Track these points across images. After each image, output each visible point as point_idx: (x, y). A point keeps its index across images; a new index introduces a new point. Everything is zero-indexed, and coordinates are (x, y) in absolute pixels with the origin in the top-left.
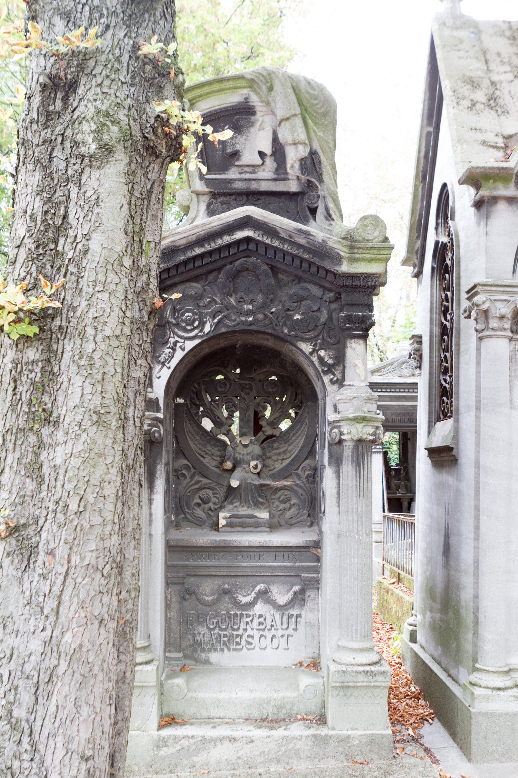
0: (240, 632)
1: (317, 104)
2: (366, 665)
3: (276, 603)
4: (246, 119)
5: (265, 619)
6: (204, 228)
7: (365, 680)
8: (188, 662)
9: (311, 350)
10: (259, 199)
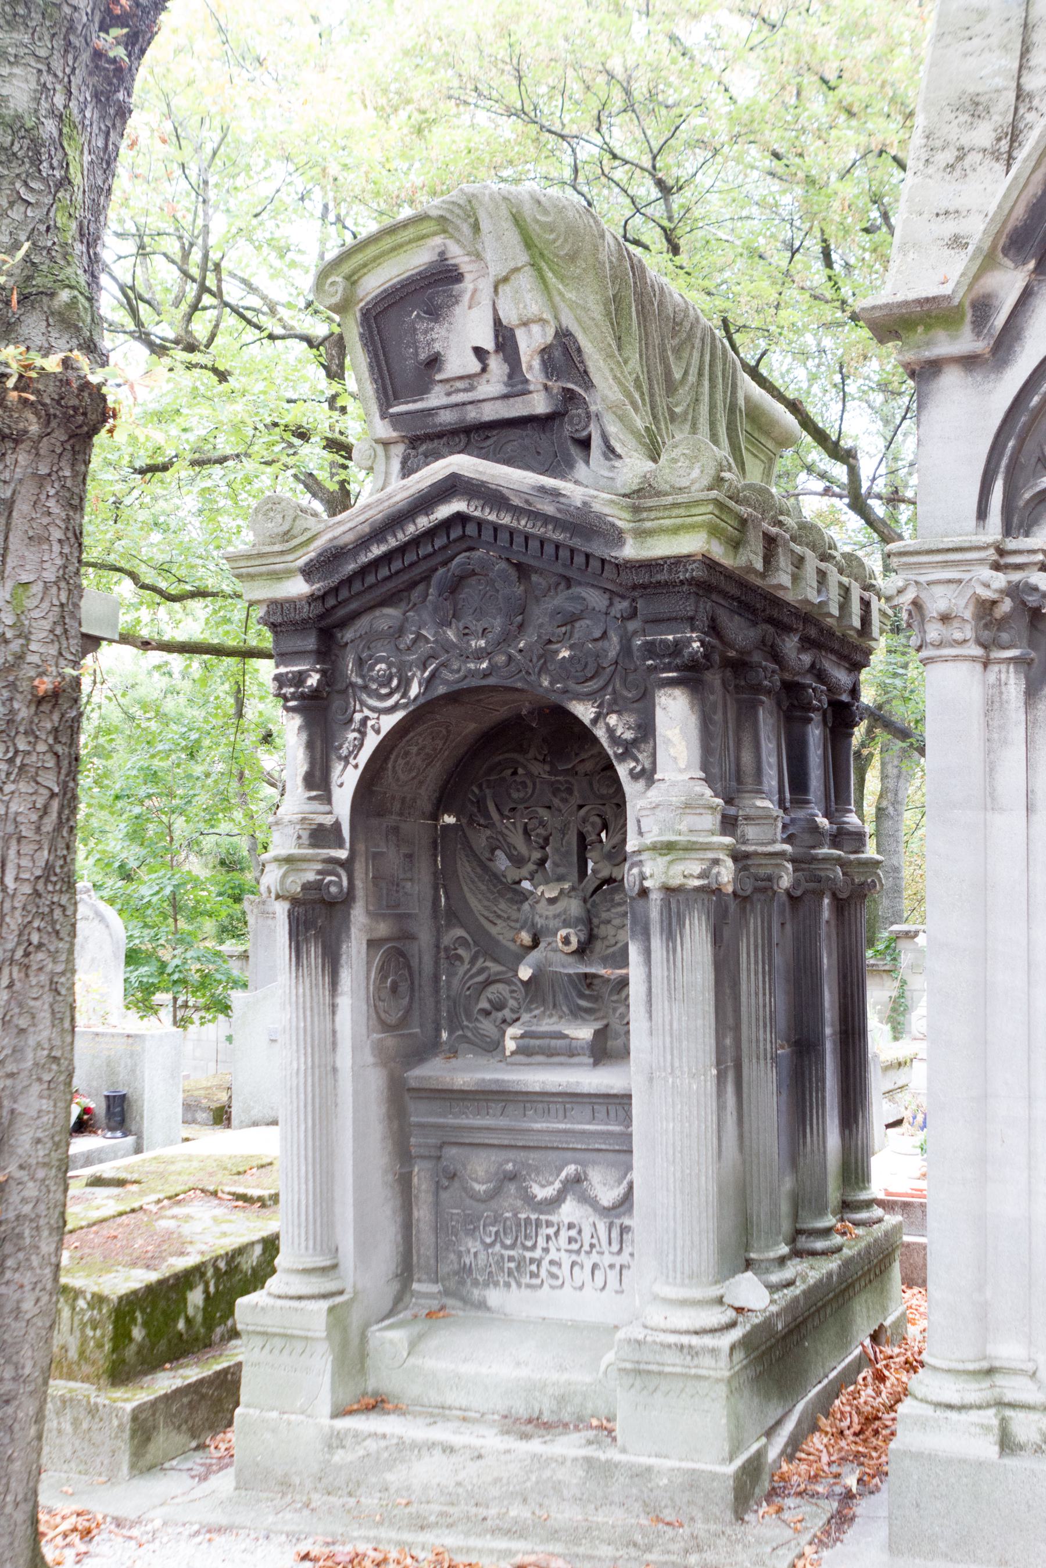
0: (537, 1254)
1: (554, 241)
2: (688, 1332)
3: (597, 1202)
4: (444, 291)
5: (580, 1232)
6: (381, 508)
7: (678, 1361)
8: (450, 1302)
9: (592, 716)
10: (488, 437)
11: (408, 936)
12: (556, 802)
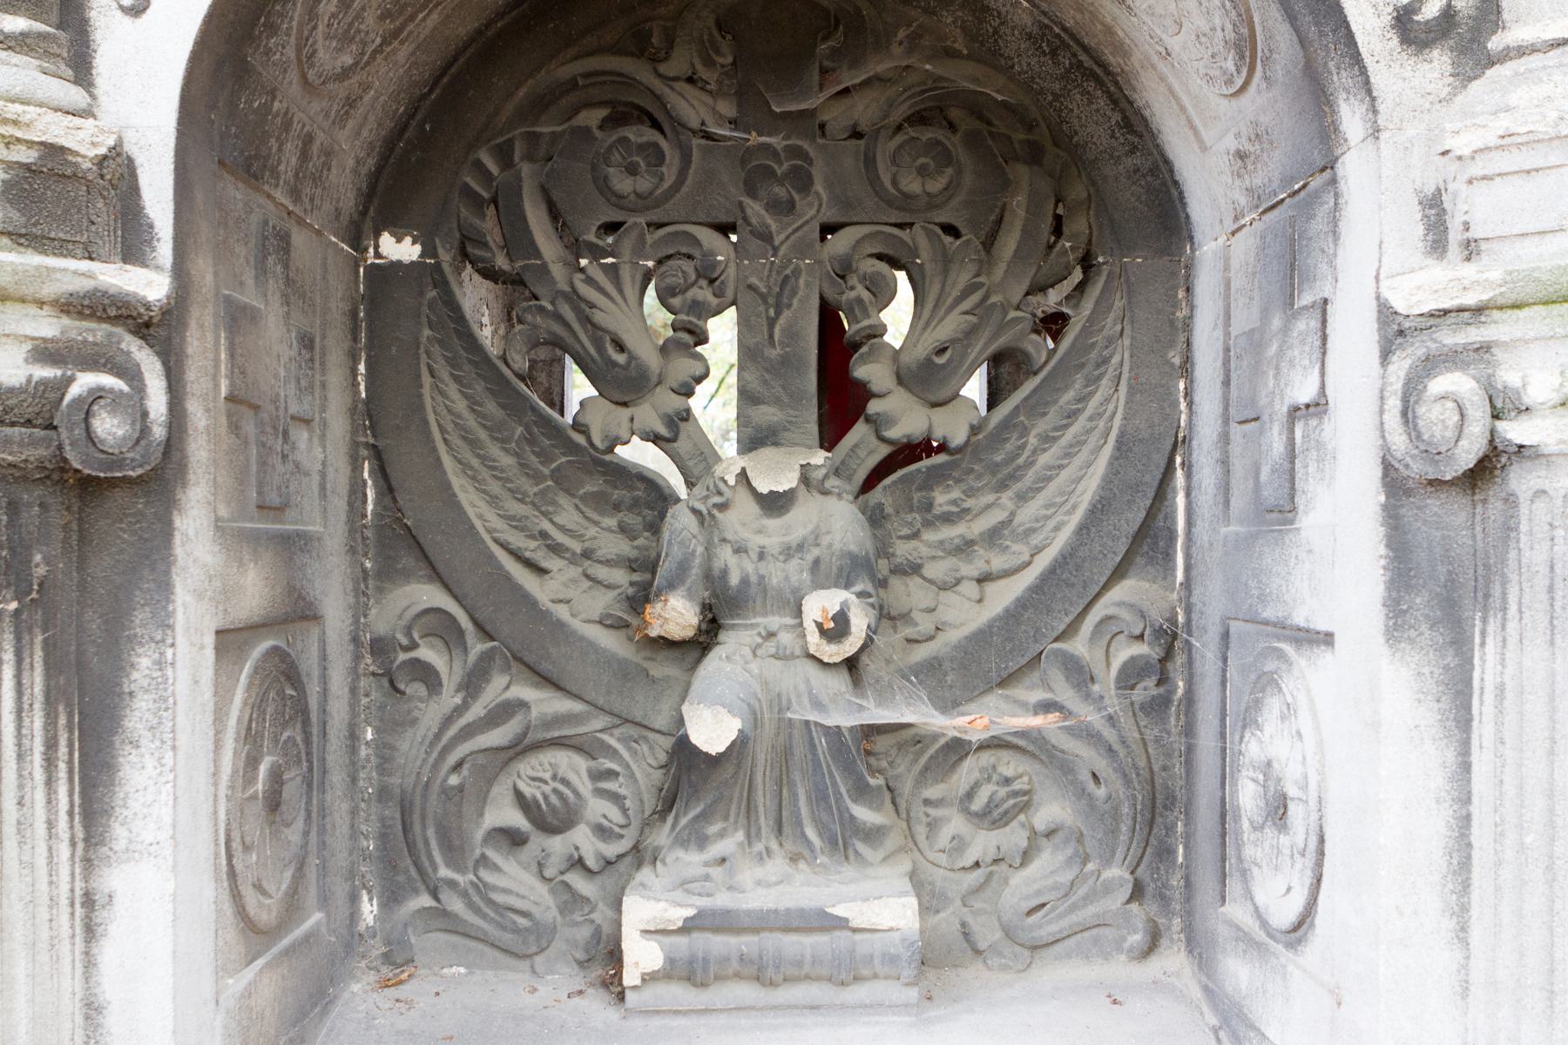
11: (298, 612)
12: (755, 210)
